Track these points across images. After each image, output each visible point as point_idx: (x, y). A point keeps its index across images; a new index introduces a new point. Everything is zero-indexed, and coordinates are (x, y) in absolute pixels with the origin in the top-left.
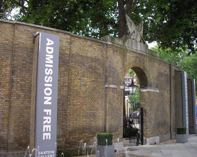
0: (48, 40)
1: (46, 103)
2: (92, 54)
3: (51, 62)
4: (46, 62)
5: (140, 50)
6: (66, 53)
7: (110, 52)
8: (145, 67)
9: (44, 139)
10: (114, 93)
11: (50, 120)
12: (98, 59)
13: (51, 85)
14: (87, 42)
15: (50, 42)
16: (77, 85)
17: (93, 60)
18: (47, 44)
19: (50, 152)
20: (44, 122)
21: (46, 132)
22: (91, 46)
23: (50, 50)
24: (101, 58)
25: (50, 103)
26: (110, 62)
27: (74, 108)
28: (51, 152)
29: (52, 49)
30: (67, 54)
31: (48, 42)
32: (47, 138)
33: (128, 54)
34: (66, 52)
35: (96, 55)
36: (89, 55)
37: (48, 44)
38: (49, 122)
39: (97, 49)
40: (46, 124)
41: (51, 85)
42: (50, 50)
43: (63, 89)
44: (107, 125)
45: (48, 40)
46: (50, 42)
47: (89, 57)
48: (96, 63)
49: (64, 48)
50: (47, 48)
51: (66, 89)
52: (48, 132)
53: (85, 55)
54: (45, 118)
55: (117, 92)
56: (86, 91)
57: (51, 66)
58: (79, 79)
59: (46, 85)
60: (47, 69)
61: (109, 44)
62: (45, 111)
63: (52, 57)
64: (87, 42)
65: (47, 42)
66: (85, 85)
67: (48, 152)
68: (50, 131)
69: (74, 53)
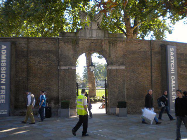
0: (3, 46)
1: (2, 82)
2: (46, 48)
3: (5, 58)
4: (2, 59)
5: (95, 36)
6: (24, 51)
7: (62, 44)
8: (104, 49)
9: (1, 103)
10: (66, 73)
11: (4, 92)
12: (52, 50)
13: (5, 72)
14: (41, 40)
15: (4, 47)
16: (35, 70)
17: (46, 52)
18: (2, 49)
19: (173, 67)
20: (1, 93)
21: (173, 95)
22: (45, 42)
23: (4, 52)
24: (54, 49)
25: (4, 83)
26: (61, 51)
27: (33, 84)
28: (173, 68)
29: (5, 51)
30: (25, 51)
31: (3, 47)
32: (2, 103)
33: (80, 42)
34: (24, 50)
35: (50, 48)
36: (44, 48)
37: (3, 48)
38: (4, 93)
39: (50, 44)
40: (2, 94)
41: (5, 72)
42: (4, 52)
43: (23, 73)
44: (60, 96)
45: (3, 46)
46: (4, 47)
47: (44, 50)
48: (50, 53)
49: (23, 48)
50: (3, 51)
51: (26, 73)
52: (3, 99)
53: (40, 49)
54: (1, 91)
55: (68, 72)
56: (42, 73)
57: (5, 61)
58: (36, 66)
59: (2, 72)
60: (2, 63)
61: (60, 38)
62: (2, 87)
63: (5, 55)
64: (41, 40)
65: (2, 47)
66: (41, 69)
67: (172, 62)
68: (4, 98)
69: (31, 49)
